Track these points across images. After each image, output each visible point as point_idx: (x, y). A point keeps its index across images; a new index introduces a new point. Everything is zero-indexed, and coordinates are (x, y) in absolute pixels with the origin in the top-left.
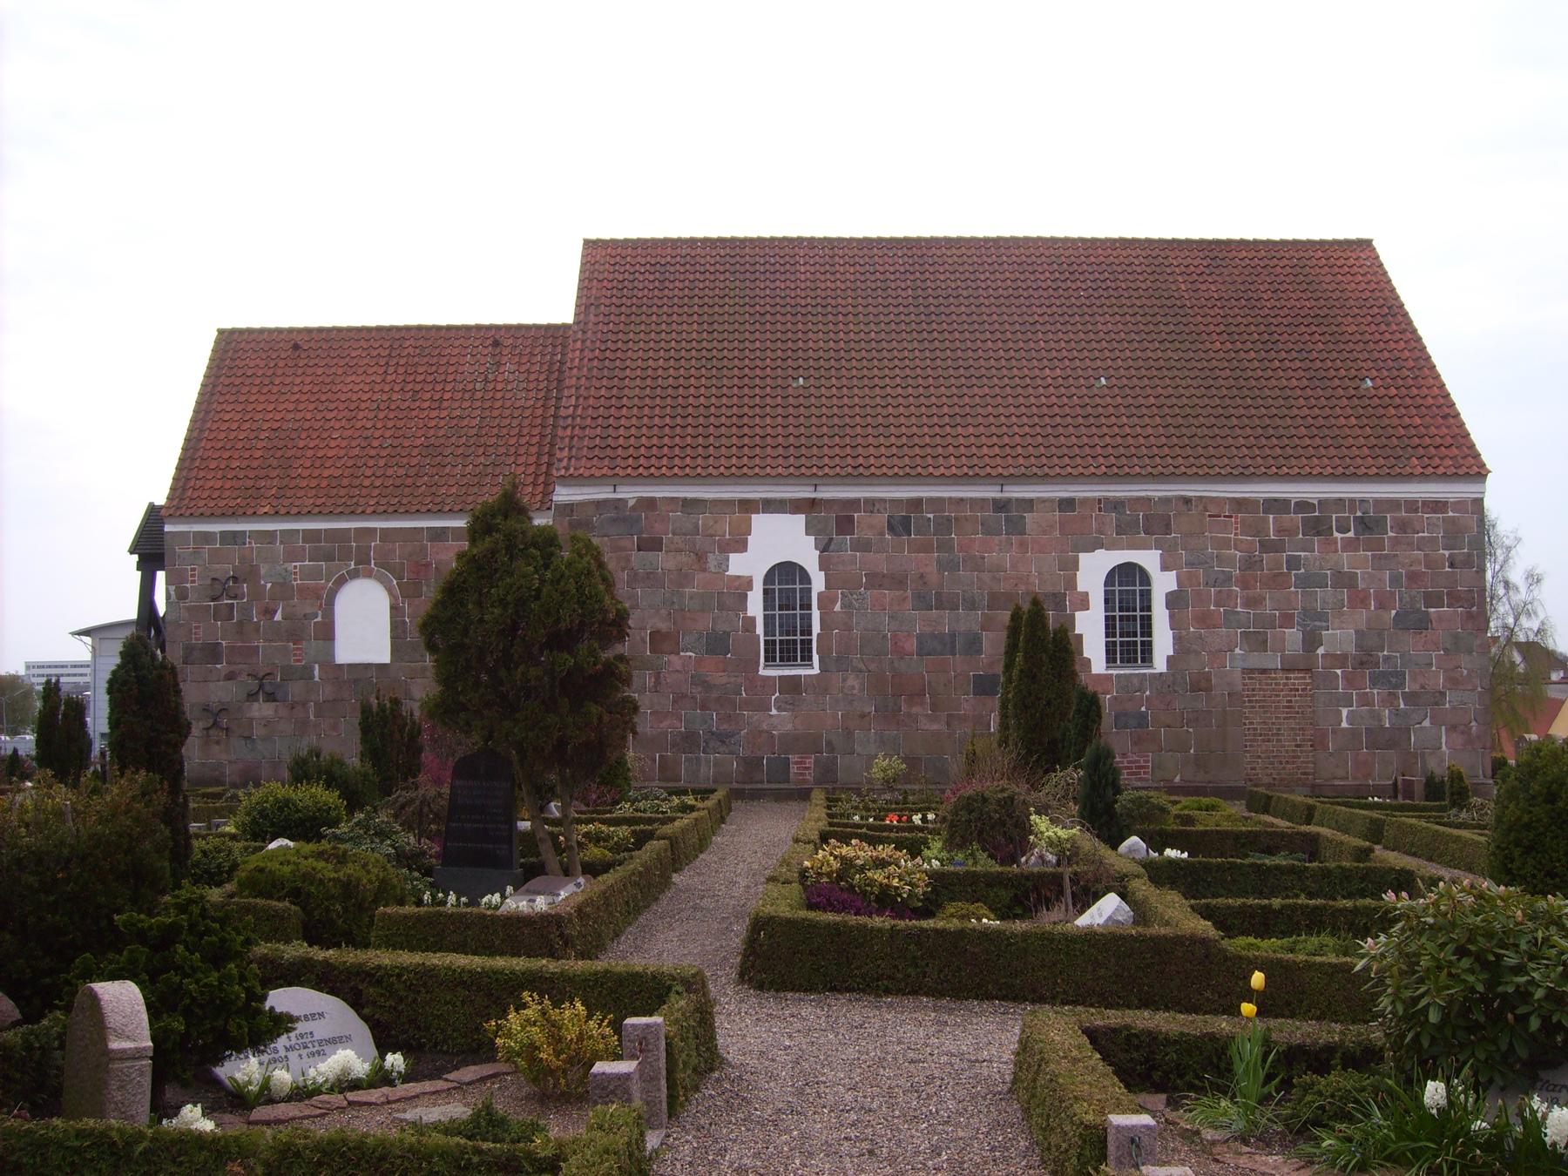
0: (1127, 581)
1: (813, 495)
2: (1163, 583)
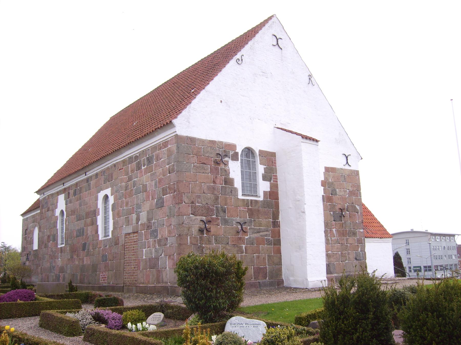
0: (106, 197)
1: (64, 187)
2: (111, 200)
